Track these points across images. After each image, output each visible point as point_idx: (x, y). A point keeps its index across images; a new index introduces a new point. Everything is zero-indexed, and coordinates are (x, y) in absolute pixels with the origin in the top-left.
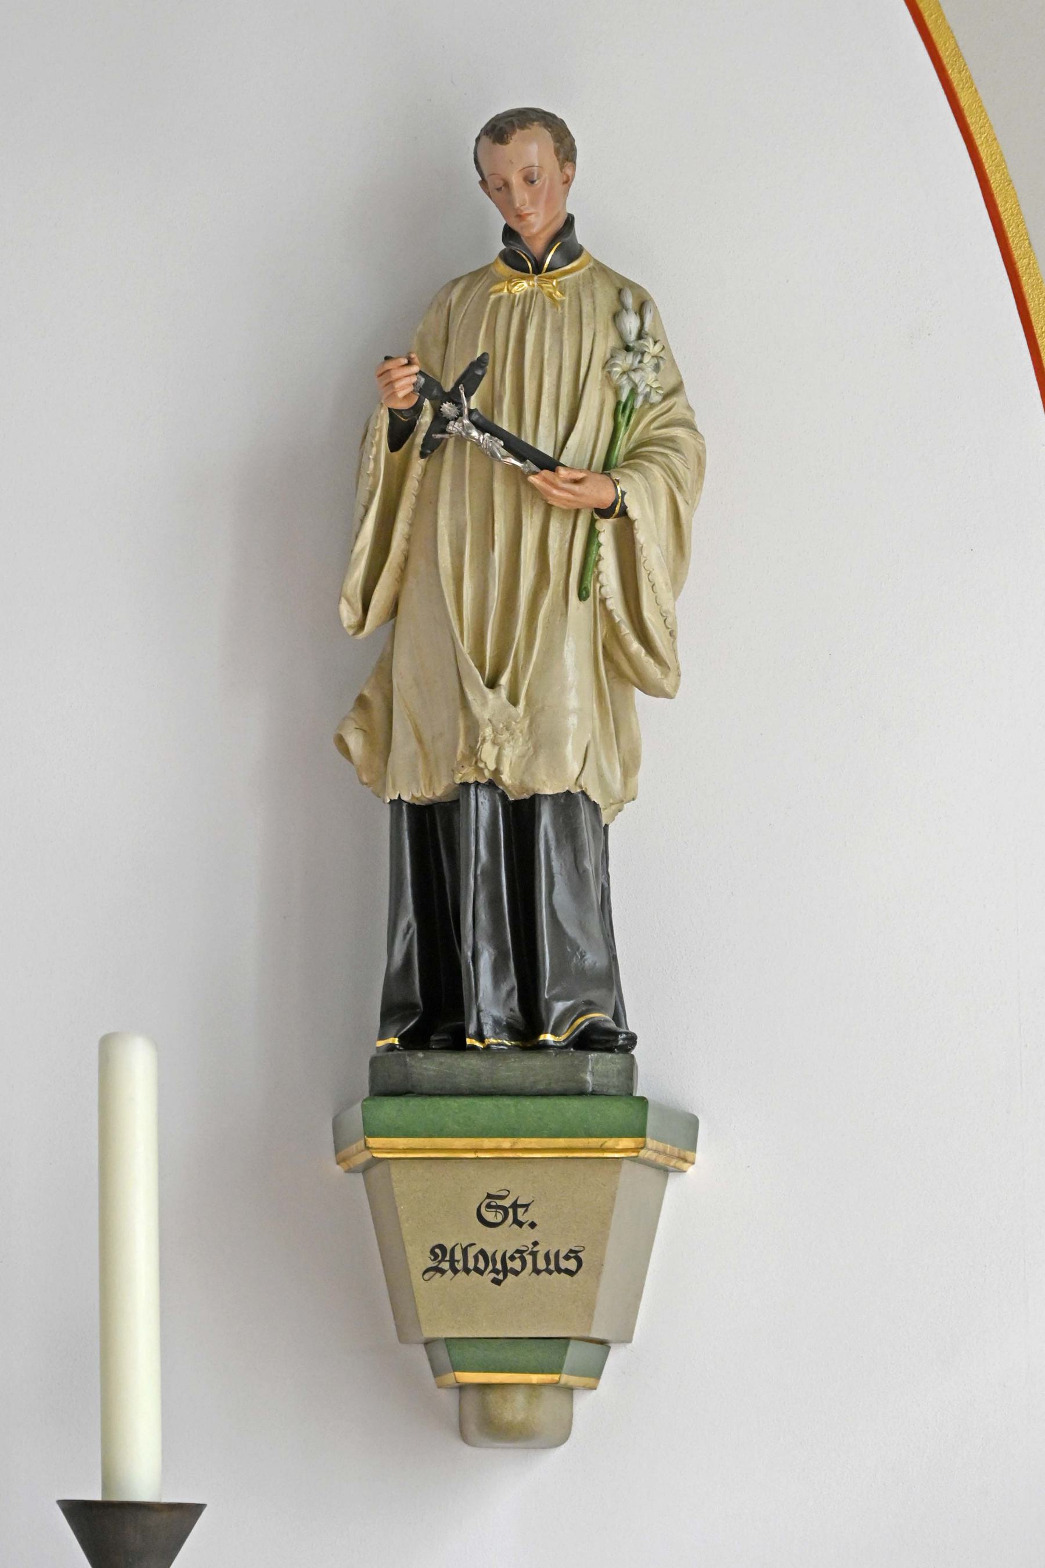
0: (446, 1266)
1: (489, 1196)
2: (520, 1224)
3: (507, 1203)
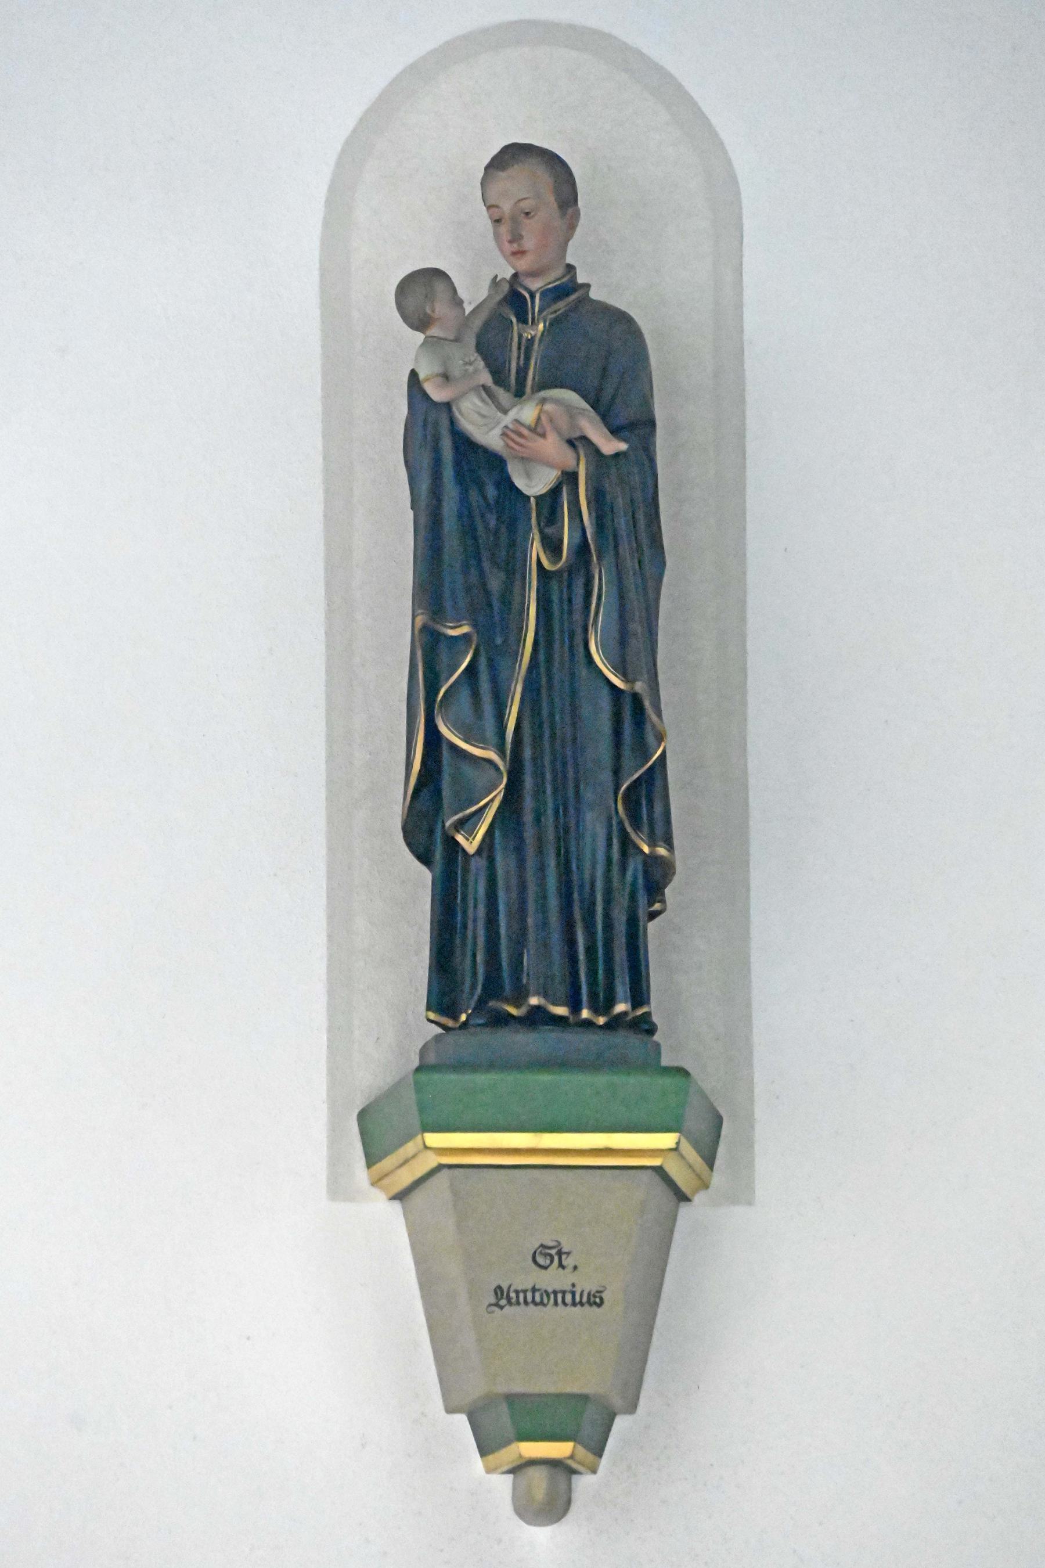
0: (503, 1302)
1: (542, 1246)
2: (563, 1267)
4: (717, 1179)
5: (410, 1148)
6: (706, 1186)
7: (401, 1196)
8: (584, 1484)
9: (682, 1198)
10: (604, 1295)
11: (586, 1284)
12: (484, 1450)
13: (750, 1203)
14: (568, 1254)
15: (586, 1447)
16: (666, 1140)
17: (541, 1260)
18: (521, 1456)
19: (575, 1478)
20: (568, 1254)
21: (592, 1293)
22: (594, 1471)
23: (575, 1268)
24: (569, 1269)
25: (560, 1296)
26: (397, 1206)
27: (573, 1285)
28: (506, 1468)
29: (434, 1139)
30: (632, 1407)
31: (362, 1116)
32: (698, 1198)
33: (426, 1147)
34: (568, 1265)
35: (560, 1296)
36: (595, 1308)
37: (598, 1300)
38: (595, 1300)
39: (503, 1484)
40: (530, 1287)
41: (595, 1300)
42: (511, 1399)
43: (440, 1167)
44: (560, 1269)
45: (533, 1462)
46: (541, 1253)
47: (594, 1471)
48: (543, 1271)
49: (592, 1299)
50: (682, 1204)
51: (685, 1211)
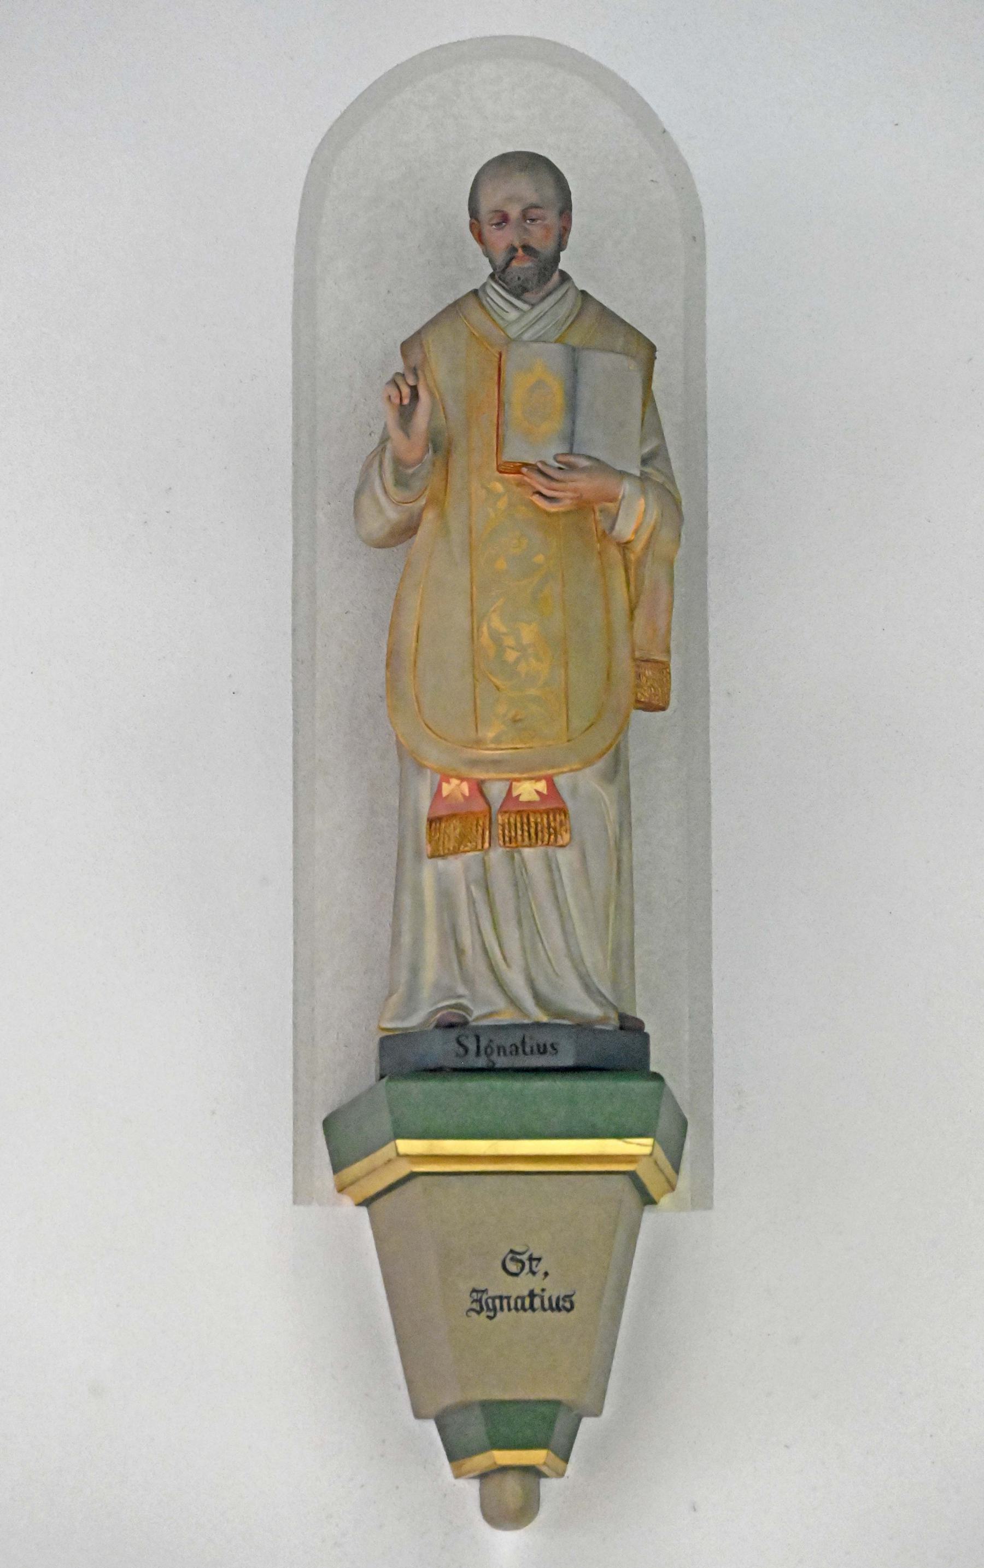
1: (512, 1251)
2: (534, 1273)
3: (524, 1258)
4: (683, 1182)
5: (386, 1152)
6: (672, 1188)
7: (367, 1203)
8: (548, 1487)
9: (648, 1200)
10: (574, 1298)
11: (554, 1290)
12: (453, 1456)
13: (709, 1207)
14: (539, 1260)
15: (556, 1454)
16: (639, 1146)
17: (513, 1267)
18: (495, 1463)
19: (544, 1482)
20: (539, 1260)
21: (561, 1298)
22: (561, 1474)
23: (546, 1274)
24: (540, 1275)
25: (505, 1302)
26: (364, 1211)
27: (543, 1290)
28: (477, 1473)
29: (405, 1146)
30: (597, 1413)
31: (326, 1124)
32: (665, 1201)
33: (398, 1155)
34: (538, 1271)
35: (505, 1302)
36: (564, 1313)
37: (568, 1305)
38: (563, 1304)
39: (471, 1489)
40: (526, 1293)
41: (563, 1304)
42: (486, 1405)
43: (412, 1176)
44: (530, 1275)
45: (504, 1469)
46: (512, 1259)
47: (561, 1474)
48: (515, 1278)
49: (561, 1303)
50: (647, 1208)
51: (649, 1217)
